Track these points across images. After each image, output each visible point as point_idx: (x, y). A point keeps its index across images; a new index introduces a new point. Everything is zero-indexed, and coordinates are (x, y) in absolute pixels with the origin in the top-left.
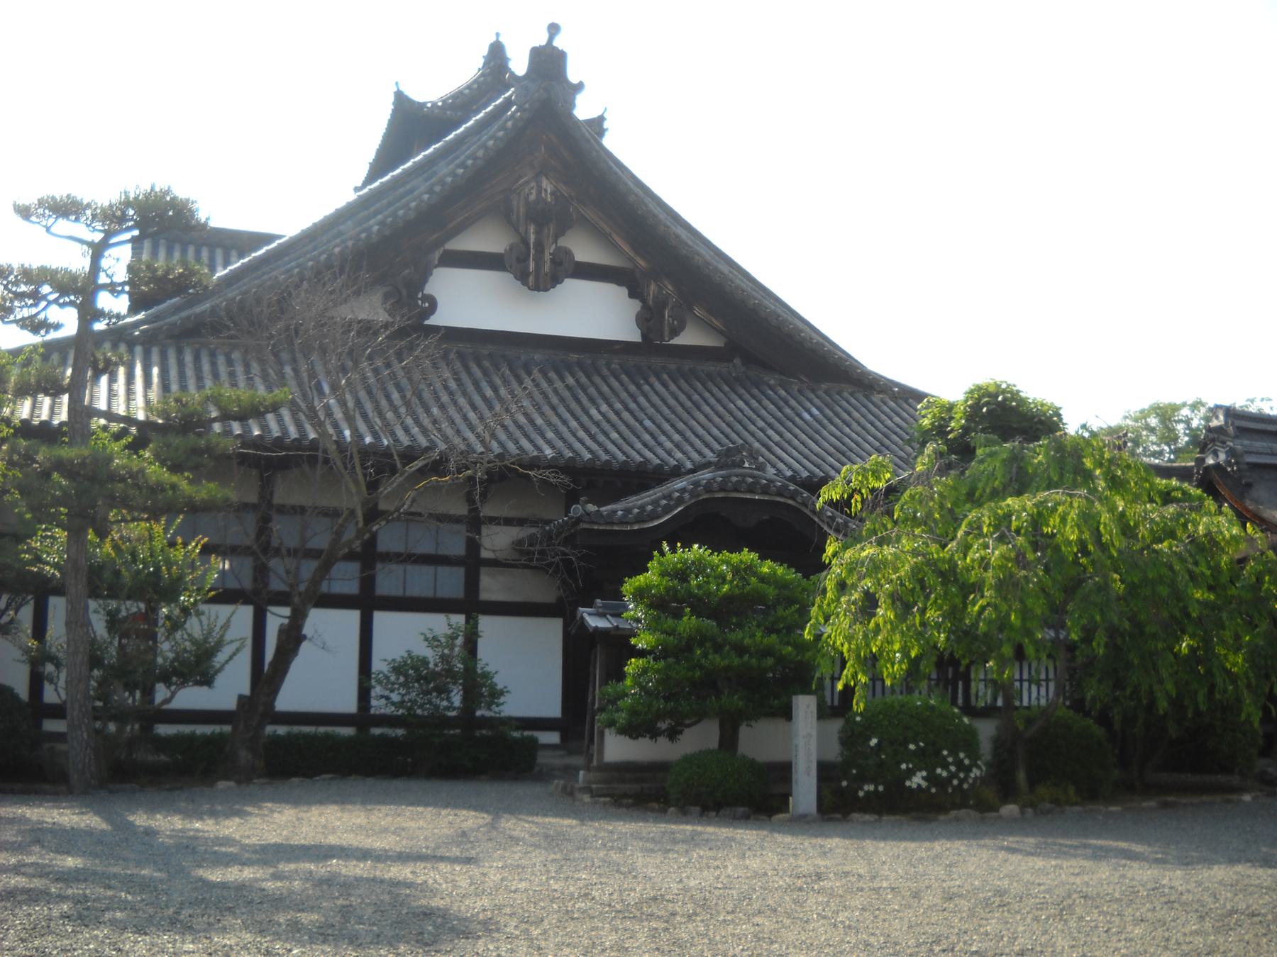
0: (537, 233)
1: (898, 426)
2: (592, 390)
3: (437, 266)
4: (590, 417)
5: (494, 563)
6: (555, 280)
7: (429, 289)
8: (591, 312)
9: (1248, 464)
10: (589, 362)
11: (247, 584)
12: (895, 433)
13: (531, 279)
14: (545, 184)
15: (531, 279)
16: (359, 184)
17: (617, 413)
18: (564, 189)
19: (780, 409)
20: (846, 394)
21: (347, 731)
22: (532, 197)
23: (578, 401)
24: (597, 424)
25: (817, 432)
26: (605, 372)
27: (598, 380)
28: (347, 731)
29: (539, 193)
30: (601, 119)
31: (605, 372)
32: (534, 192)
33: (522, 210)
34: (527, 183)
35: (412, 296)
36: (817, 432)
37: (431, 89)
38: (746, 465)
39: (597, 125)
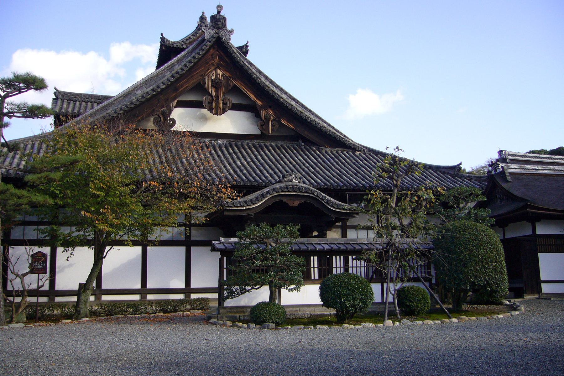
0: (216, 92)
1: (365, 164)
2: (239, 154)
3: (175, 107)
4: (236, 164)
5: (196, 225)
6: (224, 111)
7: (172, 116)
8: (231, 123)
9: (510, 173)
10: (240, 143)
11: (183, 237)
12: (364, 167)
13: (214, 111)
14: (220, 72)
15: (214, 111)
16: (549, 149)
17: (248, 163)
18: (227, 74)
19: (316, 159)
20: (345, 152)
21: (137, 297)
22: (213, 78)
23: (233, 158)
24: (239, 167)
25: (330, 168)
26: (246, 147)
27: (243, 150)
28: (137, 297)
29: (216, 76)
30: (246, 46)
31: (246, 147)
32: (214, 75)
33: (210, 83)
34: (211, 71)
35: (165, 119)
36: (330, 168)
37: (176, 36)
38: (294, 181)
39: (244, 50)
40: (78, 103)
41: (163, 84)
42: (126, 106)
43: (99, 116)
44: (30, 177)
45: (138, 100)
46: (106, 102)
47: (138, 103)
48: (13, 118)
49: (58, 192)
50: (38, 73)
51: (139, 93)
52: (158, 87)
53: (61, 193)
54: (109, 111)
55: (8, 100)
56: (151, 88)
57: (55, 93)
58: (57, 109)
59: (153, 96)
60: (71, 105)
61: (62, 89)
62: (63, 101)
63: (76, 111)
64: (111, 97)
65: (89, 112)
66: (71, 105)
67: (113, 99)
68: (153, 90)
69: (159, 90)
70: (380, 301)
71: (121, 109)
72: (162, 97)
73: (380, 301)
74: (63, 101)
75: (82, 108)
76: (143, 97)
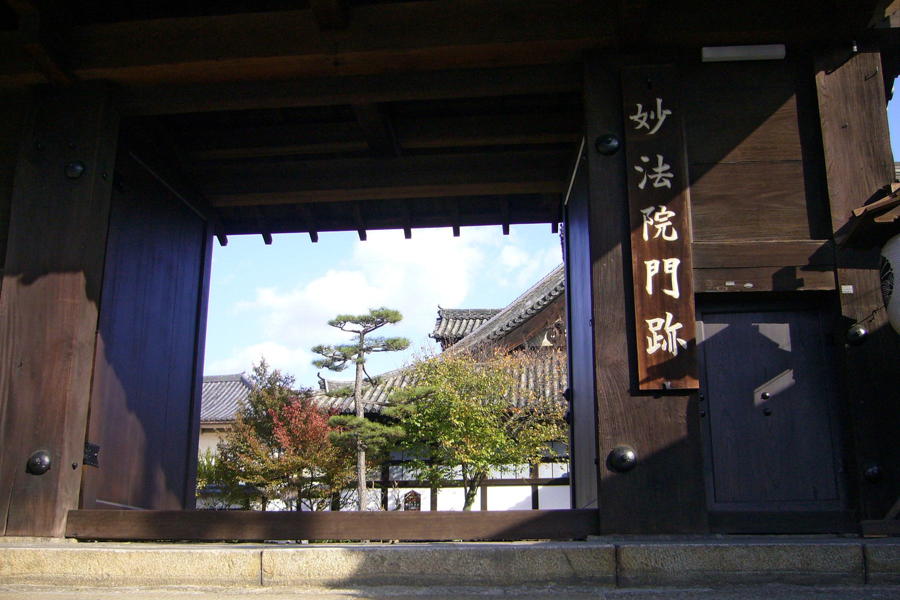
40: (465, 321)
41: (556, 290)
42: (514, 322)
43: (484, 337)
44: (386, 411)
45: (526, 313)
46: (500, 314)
47: (527, 316)
48: (372, 353)
49: (419, 425)
50: (391, 307)
51: (529, 304)
52: (550, 295)
53: (422, 425)
54: (494, 329)
55: (367, 336)
56: (543, 296)
57: (439, 312)
58: (439, 333)
59: (545, 306)
60: (457, 325)
61: (446, 306)
62: (448, 320)
63: (460, 332)
64: (498, 311)
65: (476, 330)
66: (457, 325)
67: (503, 312)
68: (544, 299)
69: (552, 298)
70: (566, 490)
71: (508, 326)
72: (555, 305)
73: (566, 490)
74: (448, 320)
75: (469, 327)
76: (532, 308)
